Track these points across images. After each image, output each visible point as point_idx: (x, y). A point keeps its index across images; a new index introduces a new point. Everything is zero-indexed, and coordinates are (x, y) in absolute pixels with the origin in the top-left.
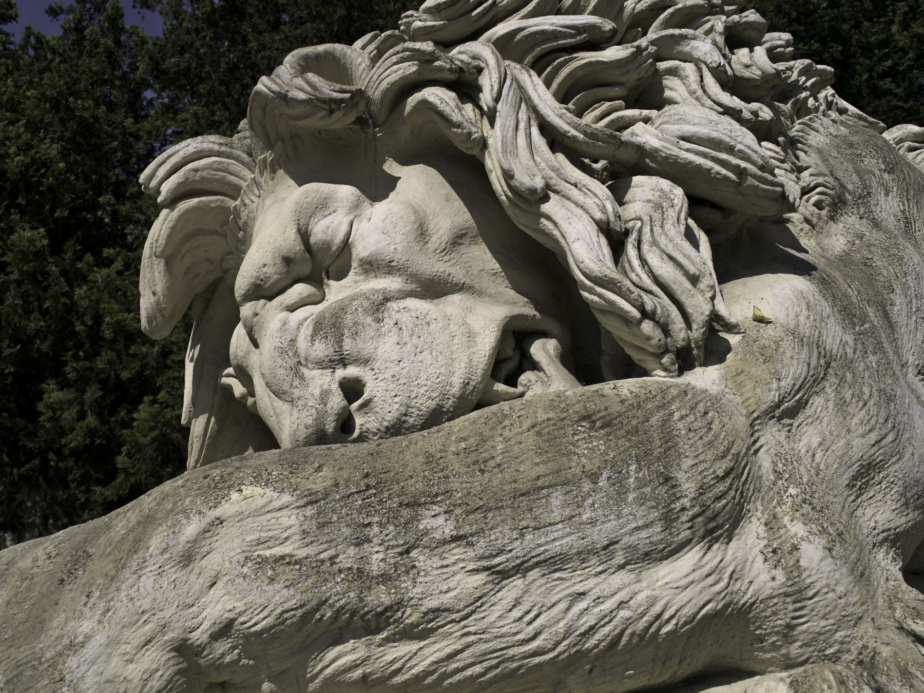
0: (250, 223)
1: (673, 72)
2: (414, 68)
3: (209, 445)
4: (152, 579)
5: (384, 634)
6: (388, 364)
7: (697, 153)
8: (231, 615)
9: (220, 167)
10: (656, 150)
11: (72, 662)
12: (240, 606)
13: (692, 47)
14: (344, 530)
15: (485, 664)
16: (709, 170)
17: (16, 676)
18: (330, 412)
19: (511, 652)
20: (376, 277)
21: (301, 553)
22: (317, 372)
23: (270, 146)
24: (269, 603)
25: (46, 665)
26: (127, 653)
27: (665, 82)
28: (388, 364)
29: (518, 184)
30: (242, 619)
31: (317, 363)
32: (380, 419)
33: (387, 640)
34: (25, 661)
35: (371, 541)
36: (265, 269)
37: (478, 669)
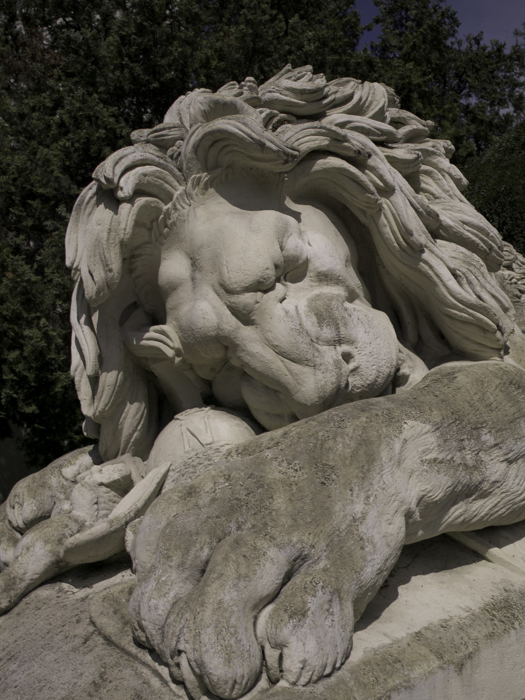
0: (178, 223)
1: (427, 173)
2: (327, 142)
3: (117, 392)
4: (390, 476)
5: (473, 498)
6: (366, 345)
7: (473, 233)
8: (422, 493)
9: (160, 175)
10: (451, 227)
11: (362, 529)
12: (429, 487)
13: (438, 161)
14: (454, 443)
15: (507, 507)
16: (478, 244)
17: (330, 542)
18: (344, 374)
19: (516, 500)
20: (328, 285)
21: (441, 457)
22: (325, 348)
23: (206, 168)
24: (438, 485)
25: (344, 533)
26: (389, 520)
27: (421, 178)
28: (366, 345)
29: (415, 240)
30: (430, 495)
31: (326, 342)
32: (365, 379)
33: (474, 500)
34: (331, 532)
35: (465, 449)
36: (268, 272)
37: (504, 510)
